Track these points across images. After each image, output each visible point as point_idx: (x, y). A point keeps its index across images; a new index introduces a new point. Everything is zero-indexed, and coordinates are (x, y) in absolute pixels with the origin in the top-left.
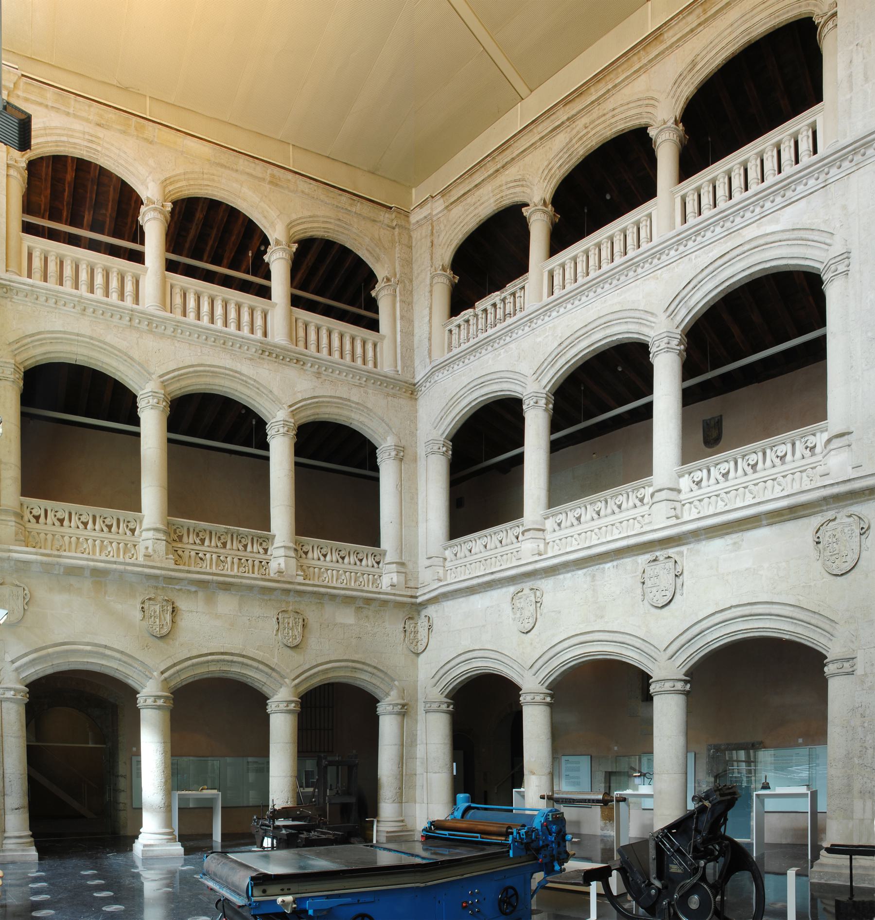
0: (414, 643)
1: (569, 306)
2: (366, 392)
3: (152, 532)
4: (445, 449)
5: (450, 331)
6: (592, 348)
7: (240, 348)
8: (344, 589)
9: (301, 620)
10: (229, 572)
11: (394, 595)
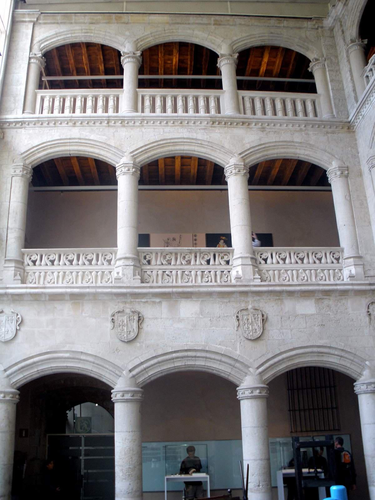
2: (307, 134)
3: (122, 261)
9: (260, 316)
11: (352, 284)
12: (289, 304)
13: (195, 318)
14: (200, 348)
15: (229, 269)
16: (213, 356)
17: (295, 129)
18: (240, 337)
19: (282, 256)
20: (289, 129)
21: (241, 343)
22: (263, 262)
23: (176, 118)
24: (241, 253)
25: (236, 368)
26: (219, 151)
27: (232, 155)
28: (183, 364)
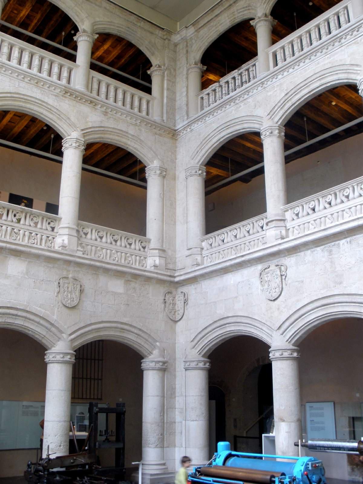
0: (173, 313)
1: (291, 70)
2: (140, 130)
4: (200, 172)
5: (202, 98)
6: (312, 93)
7: (49, 87)
8: (115, 265)
9: (79, 287)
10: (20, 242)
11: (157, 273)
12: (103, 280)
13: (21, 278)
14: (22, 308)
15: (54, 236)
16: (32, 317)
17: (132, 122)
18: (58, 303)
19: (100, 234)
20: (126, 120)
21: (58, 308)
22: (84, 236)
23: (34, 77)
24: (69, 223)
25: (51, 331)
26: (64, 121)
27: (75, 129)
28: (3, 321)
